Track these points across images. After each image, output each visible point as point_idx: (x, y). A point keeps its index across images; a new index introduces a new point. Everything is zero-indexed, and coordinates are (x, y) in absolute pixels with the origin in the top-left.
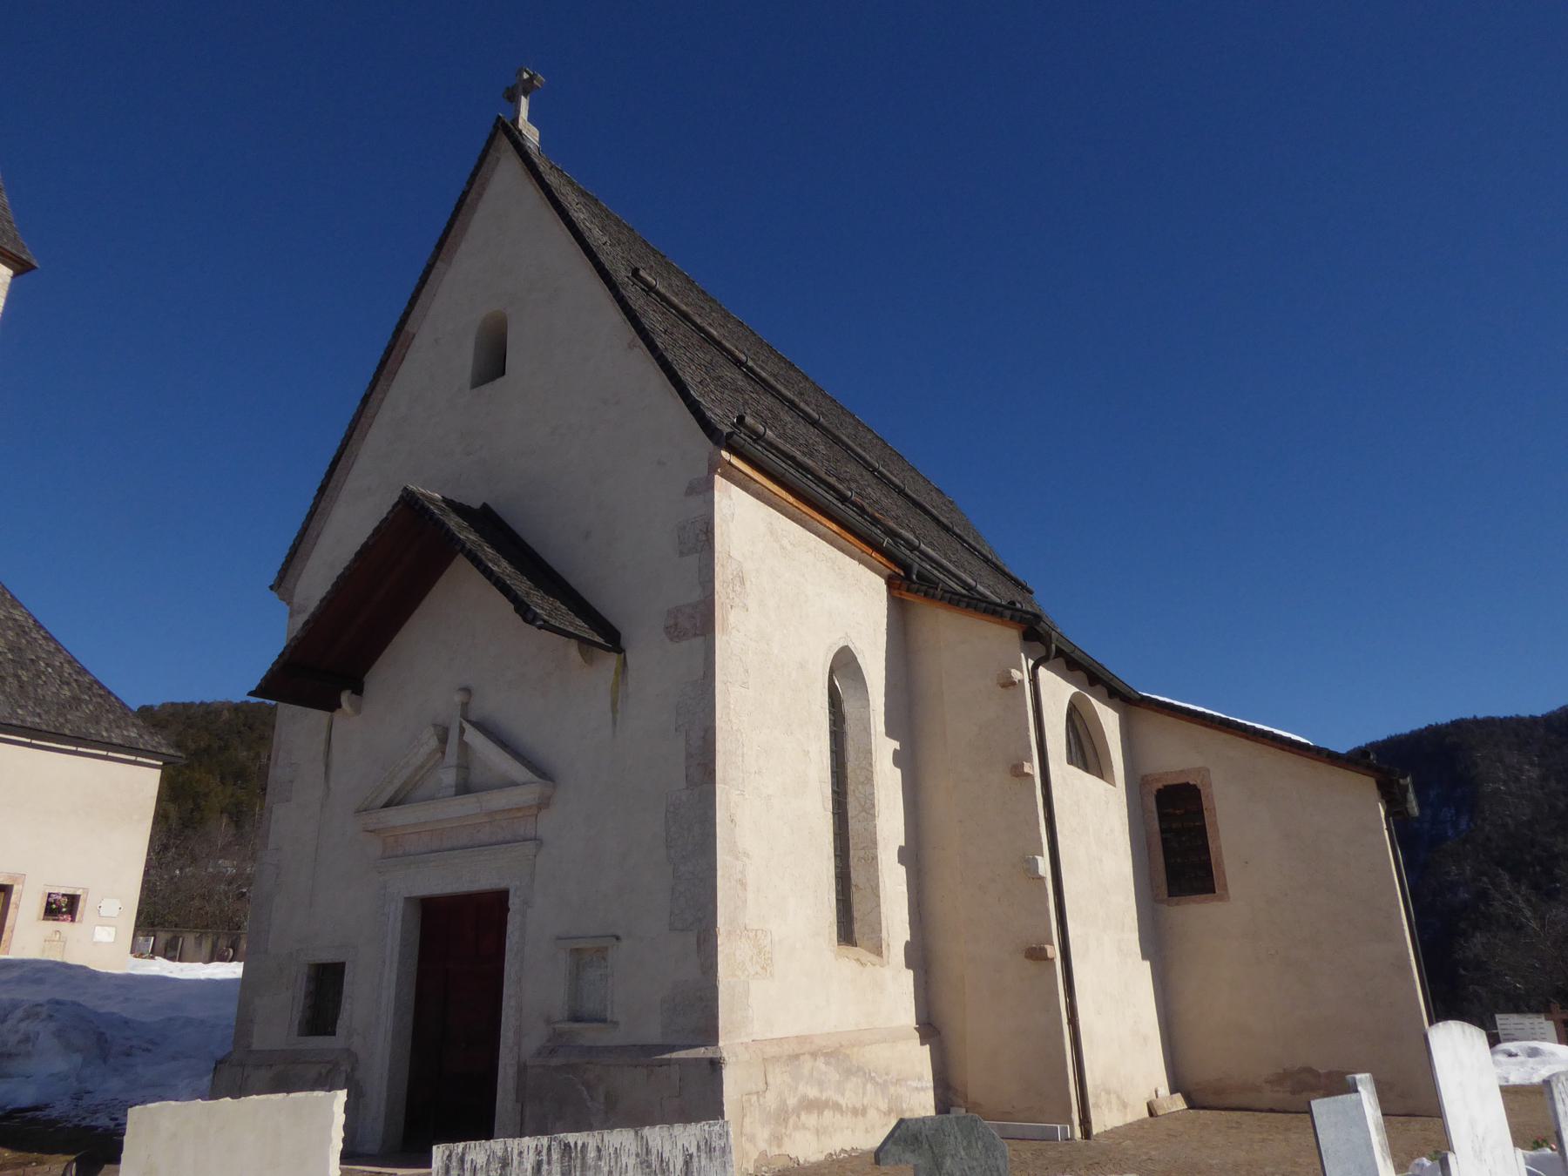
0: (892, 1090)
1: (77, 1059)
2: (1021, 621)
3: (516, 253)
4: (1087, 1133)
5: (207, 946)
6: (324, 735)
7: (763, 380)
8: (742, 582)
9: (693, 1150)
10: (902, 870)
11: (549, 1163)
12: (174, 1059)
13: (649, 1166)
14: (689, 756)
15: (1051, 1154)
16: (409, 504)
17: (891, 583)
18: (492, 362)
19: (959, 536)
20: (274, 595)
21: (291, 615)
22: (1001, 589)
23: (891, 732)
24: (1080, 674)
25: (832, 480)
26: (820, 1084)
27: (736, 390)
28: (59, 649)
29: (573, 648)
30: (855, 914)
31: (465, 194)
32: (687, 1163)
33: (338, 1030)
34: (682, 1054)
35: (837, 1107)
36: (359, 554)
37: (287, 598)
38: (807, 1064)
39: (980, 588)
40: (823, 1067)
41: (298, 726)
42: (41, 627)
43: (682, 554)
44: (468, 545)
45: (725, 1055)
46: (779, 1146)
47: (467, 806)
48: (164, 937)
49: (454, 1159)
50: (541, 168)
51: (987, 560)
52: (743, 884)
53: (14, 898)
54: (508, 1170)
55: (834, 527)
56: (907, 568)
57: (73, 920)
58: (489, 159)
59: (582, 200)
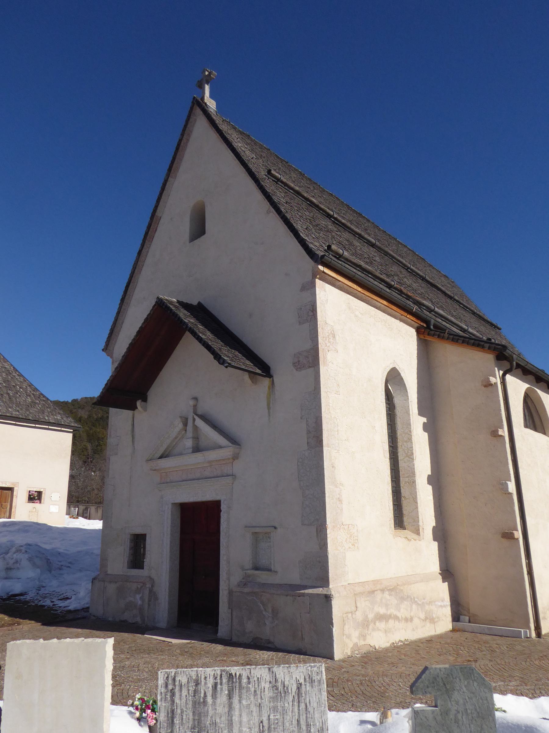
0: (427, 607)
1: (38, 571)
2: (495, 349)
3: (208, 169)
4: (539, 635)
5: (100, 512)
6: (130, 422)
7: (343, 224)
8: (334, 337)
9: (302, 681)
10: (430, 488)
11: (221, 684)
12: (80, 571)
13: (277, 689)
14: (309, 432)
15: (518, 648)
16: (161, 306)
17: (419, 331)
18: (199, 229)
19: (457, 301)
20: (104, 353)
21: (113, 363)
22: (482, 328)
23: (421, 413)
24: (531, 377)
25: (383, 277)
26: (387, 606)
27: (328, 231)
28: (25, 380)
29: (246, 376)
30: (404, 512)
31: (180, 141)
32: (299, 688)
33: (145, 567)
34: (310, 591)
35: (396, 618)
36: (139, 332)
37: (110, 355)
38: (379, 596)
39: (470, 330)
40: (388, 597)
41: (119, 418)
42: (17, 370)
43: (300, 323)
44: (190, 325)
45: (333, 593)
46: (364, 640)
47: (199, 457)
48: (82, 507)
49: (170, 679)
50: (217, 122)
51: (474, 313)
52: (340, 500)
53: (15, 493)
54: (199, 687)
55: (385, 303)
56: (427, 322)
57: (40, 503)
58: (191, 120)
59: (240, 136)
